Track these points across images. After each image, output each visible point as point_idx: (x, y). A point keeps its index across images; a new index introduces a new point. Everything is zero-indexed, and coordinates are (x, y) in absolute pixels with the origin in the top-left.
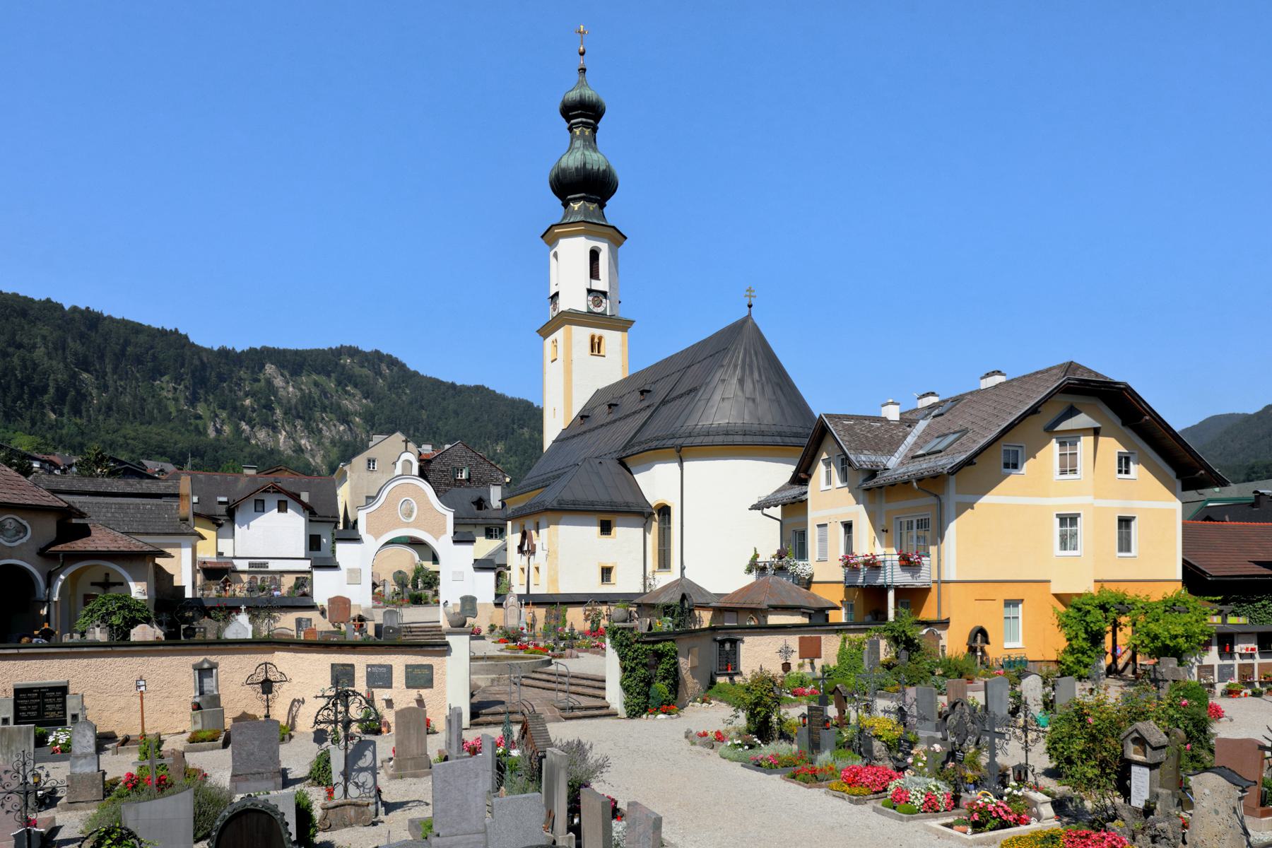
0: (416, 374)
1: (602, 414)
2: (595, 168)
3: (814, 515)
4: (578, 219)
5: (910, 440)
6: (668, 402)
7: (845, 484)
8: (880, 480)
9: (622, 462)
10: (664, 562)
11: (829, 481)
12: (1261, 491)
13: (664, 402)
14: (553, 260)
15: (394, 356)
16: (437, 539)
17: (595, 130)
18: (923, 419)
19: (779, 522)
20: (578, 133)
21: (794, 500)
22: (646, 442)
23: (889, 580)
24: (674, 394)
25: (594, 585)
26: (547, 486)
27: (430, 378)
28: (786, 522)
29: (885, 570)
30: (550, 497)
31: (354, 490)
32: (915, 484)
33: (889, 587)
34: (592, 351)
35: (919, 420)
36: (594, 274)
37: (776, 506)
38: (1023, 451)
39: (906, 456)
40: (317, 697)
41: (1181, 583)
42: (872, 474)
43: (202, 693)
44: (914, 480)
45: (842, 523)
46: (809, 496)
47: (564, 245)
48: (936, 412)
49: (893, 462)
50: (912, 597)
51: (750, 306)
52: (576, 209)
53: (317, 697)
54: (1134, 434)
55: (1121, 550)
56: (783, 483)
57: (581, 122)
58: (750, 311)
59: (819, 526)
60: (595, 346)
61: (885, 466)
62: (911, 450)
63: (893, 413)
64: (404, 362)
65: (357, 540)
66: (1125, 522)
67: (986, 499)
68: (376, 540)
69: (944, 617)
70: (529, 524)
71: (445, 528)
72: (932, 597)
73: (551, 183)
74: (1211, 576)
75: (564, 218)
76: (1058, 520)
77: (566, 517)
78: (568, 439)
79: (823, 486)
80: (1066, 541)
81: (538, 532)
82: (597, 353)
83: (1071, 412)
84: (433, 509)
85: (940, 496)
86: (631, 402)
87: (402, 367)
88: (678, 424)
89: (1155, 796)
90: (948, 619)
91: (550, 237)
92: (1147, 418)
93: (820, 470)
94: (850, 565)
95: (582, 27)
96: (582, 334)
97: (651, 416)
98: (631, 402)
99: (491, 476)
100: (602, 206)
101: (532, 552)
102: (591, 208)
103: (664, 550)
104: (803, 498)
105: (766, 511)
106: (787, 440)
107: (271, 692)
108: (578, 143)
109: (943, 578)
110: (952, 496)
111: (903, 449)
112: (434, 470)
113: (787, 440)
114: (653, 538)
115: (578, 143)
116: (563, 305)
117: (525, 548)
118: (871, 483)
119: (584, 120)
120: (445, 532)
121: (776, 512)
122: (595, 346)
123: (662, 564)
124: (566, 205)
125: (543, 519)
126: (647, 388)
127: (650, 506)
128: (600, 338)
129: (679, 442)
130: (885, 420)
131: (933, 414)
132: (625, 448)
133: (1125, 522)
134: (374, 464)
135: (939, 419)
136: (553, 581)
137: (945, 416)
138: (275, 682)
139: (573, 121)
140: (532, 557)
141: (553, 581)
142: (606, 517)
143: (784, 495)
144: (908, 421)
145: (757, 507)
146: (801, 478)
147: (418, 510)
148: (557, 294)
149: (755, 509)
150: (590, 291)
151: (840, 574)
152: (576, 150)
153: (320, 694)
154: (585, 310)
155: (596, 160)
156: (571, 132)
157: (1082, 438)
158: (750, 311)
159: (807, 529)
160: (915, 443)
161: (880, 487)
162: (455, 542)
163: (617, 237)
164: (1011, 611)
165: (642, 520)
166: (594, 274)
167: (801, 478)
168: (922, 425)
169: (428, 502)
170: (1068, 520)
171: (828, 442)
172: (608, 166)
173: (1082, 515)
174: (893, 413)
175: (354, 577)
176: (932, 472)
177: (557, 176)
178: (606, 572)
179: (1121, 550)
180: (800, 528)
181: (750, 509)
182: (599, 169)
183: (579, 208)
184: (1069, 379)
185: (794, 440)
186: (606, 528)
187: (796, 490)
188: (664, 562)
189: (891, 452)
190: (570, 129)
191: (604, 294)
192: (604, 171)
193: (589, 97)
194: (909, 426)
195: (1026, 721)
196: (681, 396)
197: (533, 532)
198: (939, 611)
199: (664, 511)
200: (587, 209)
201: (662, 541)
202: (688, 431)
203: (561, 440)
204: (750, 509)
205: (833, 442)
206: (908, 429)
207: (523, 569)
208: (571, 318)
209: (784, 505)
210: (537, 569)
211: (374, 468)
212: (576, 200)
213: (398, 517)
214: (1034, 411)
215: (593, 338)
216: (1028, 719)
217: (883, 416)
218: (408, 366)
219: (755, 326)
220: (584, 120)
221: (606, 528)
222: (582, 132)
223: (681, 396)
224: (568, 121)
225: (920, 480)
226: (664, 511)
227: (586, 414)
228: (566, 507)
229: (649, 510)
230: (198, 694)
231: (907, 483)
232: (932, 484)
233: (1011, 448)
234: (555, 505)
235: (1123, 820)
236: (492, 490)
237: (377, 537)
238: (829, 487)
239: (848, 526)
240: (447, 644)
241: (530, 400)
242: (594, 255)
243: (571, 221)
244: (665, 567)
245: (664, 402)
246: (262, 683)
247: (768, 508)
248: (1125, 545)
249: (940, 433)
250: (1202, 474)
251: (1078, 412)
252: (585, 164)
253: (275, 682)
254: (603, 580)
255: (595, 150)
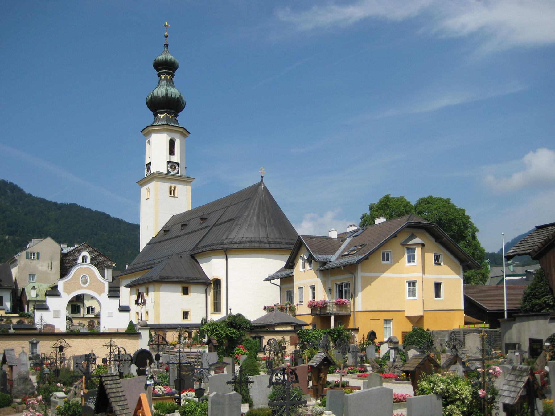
0: (30, 195)
1: (176, 231)
2: (173, 96)
3: (297, 283)
4: (163, 123)
5: (343, 247)
6: (217, 225)
7: (311, 268)
8: (327, 266)
9: (193, 257)
10: (217, 308)
11: (303, 267)
12: (529, 271)
13: (215, 225)
14: (147, 145)
15: (15, 183)
16: (100, 295)
17: (173, 76)
18: (348, 238)
19: (279, 287)
20: (163, 77)
21: (286, 276)
22: (207, 246)
23: (331, 311)
24: (220, 222)
25: (179, 320)
26: (152, 268)
27: (40, 198)
28: (284, 286)
29: (329, 307)
30: (155, 273)
31: (21, 271)
32: (342, 268)
33: (332, 314)
34: (170, 194)
35: (347, 238)
36: (172, 152)
37: (277, 279)
38: (391, 253)
39: (340, 255)
40: (104, 346)
41: (463, 311)
42: (324, 263)
43: (32, 353)
44: (342, 266)
45: (310, 286)
46: (294, 274)
47: (155, 138)
48: (355, 234)
49: (333, 258)
50: (342, 319)
51: (262, 177)
52: (162, 117)
53: (104, 346)
54: (440, 245)
55: (436, 297)
56: (281, 268)
57: (166, 72)
58: (262, 180)
59: (299, 288)
60: (172, 192)
61: (330, 260)
62: (342, 252)
63: (334, 235)
64: (22, 187)
65: (58, 295)
66: (438, 285)
67: (384, 275)
68: (68, 295)
69: (356, 327)
70: (142, 289)
71: (104, 290)
72: (352, 318)
73: (147, 103)
74: (488, 310)
75: (154, 122)
76: (407, 284)
77: (164, 287)
78: (156, 243)
79: (301, 269)
80: (412, 293)
81: (147, 294)
82: (173, 195)
83: (413, 237)
84: (98, 280)
85: (354, 274)
86: (194, 224)
87: (20, 191)
88: (224, 237)
89: (395, 357)
90: (358, 328)
91: (146, 132)
92: (445, 239)
93: (300, 262)
94: (313, 307)
95: (166, 23)
96: (165, 186)
97: (208, 232)
98: (194, 224)
99: (104, 263)
100: (176, 116)
101: (144, 303)
102: (170, 117)
103: (217, 303)
104: (291, 275)
105: (272, 281)
106: (282, 246)
107: (62, 351)
108: (163, 83)
109: (356, 310)
110: (361, 274)
111: (339, 252)
112: (69, 260)
113: (282, 246)
114: (210, 298)
115: (163, 83)
116: (153, 169)
117: (140, 301)
118: (323, 268)
119: (167, 71)
120: (104, 292)
121: (278, 282)
122: (172, 192)
123: (216, 309)
124: (156, 115)
125: (151, 287)
126: (205, 217)
127: (210, 280)
128: (175, 188)
129: (225, 246)
130: (330, 238)
131: (353, 235)
132: (194, 249)
133: (438, 285)
134: (34, 256)
135: (356, 238)
136: (157, 316)
137: (359, 236)
138: (65, 347)
139: (160, 71)
140: (144, 307)
141: (157, 316)
142: (185, 285)
143: (281, 273)
144: (342, 238)
145: (268, 279)
146: (290, 265)
147: (90, 280)
148: (150, 163)
149: (267, 280)
150: (169, 162)
151: (309, 311)
152: (162, 87)
153: (105, 345)
154: (166, 172)
155: (174, 92)
156: (159, 77)
157: (416, 248)
158: (262, 180)
159: (293, 290)
160: (344, 249)
161: (328, 269)
162: (109, 297)
163: (185, 133)
164: (387, 325)
165: (203, 288)
166: (172, 152)
167: (290, 265)
168: (348, 240)
169: (95, 277)
170: (412, 284)
171: (303, 249)
172: (180, 96)
173: (417, 281)
174: (334, 235)
175: (57, 314)
176: (349, 263)
177: (151, 99)
178: (186, 314)
179: (436, 297)
180: (290, 290)
181: (264, 281)
182: (175, 97)
183: (163, 117)
184: (409, 222)
185: (287, 246)
186: (185, 291)
187: (288, 272)
188: (217, 308)
189: (333, 253)
190: (159, 75)
191: (178, 164)
192: (178, 98)
193: (170, 59)
194: (342, 241)
195: (364, 342)
196: (225, 222)
197: (145, 294)
198: (355, 324)
199: (217, 282)
200: (168, 118)
201: (215, 298)
202: (230, 240)
203: (151, 244)
204: (264, 281)
205: (305, 247)
206: (341, 242)
207: (138, 313)
208: (159, 176)
209: (281, 278)
210: (147, 313)
211: (34, 258)
212: (161, 113)
213: (80, 284)
214: (395, 236)
215: (170, 188)
216: (364, 341)
217: (329, 236)
218: (24, 190)
219: (266, 189)
220: (167, 71)
221: (185, 291)
222: (166, 77)
223: (225, 222)
224: (158, 71)
225: (345, 266)
226: (217, 282)
227: (167, 229)
228: (163, 280)
229: (209, 281)
230: (31, 353)
231: (339, 267)
232: (351, 268)
233: (386, 252)
234: (158, 278)
235: (388, 365)
236: (106, 271)
237: (69, 293)
238: (304, 270)
239: (313, 288)
240: (139, 334)
241: (31, 194)
242: (172, 143)
243: (159, 124)
244: (217, 311)
245: (215, 225)
246: (59, 347)
247: (273, 280)
248: (438, 295)
249: (356, 245)
250: (469, 263)
251: (416, 237)
252: (167, 94)
253: (65, 347)
254: (184, 319)
255: (173, 87)
